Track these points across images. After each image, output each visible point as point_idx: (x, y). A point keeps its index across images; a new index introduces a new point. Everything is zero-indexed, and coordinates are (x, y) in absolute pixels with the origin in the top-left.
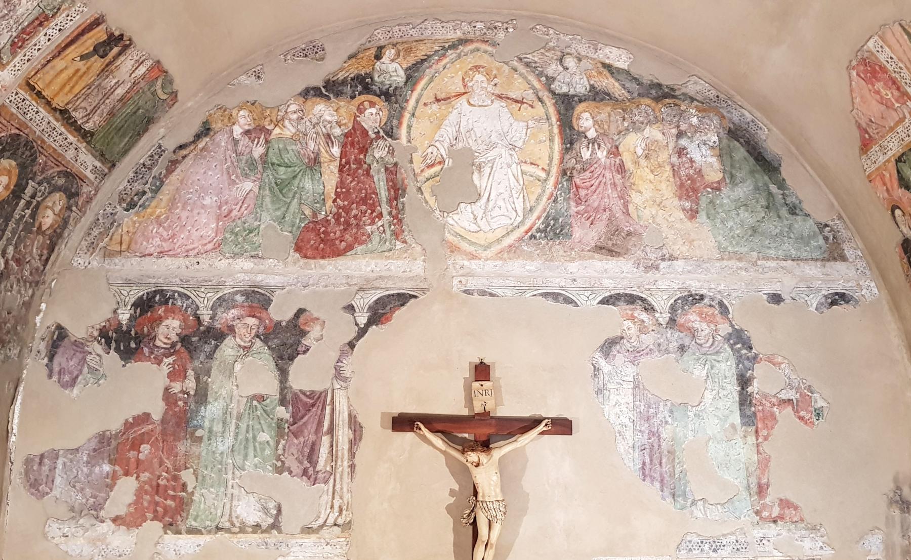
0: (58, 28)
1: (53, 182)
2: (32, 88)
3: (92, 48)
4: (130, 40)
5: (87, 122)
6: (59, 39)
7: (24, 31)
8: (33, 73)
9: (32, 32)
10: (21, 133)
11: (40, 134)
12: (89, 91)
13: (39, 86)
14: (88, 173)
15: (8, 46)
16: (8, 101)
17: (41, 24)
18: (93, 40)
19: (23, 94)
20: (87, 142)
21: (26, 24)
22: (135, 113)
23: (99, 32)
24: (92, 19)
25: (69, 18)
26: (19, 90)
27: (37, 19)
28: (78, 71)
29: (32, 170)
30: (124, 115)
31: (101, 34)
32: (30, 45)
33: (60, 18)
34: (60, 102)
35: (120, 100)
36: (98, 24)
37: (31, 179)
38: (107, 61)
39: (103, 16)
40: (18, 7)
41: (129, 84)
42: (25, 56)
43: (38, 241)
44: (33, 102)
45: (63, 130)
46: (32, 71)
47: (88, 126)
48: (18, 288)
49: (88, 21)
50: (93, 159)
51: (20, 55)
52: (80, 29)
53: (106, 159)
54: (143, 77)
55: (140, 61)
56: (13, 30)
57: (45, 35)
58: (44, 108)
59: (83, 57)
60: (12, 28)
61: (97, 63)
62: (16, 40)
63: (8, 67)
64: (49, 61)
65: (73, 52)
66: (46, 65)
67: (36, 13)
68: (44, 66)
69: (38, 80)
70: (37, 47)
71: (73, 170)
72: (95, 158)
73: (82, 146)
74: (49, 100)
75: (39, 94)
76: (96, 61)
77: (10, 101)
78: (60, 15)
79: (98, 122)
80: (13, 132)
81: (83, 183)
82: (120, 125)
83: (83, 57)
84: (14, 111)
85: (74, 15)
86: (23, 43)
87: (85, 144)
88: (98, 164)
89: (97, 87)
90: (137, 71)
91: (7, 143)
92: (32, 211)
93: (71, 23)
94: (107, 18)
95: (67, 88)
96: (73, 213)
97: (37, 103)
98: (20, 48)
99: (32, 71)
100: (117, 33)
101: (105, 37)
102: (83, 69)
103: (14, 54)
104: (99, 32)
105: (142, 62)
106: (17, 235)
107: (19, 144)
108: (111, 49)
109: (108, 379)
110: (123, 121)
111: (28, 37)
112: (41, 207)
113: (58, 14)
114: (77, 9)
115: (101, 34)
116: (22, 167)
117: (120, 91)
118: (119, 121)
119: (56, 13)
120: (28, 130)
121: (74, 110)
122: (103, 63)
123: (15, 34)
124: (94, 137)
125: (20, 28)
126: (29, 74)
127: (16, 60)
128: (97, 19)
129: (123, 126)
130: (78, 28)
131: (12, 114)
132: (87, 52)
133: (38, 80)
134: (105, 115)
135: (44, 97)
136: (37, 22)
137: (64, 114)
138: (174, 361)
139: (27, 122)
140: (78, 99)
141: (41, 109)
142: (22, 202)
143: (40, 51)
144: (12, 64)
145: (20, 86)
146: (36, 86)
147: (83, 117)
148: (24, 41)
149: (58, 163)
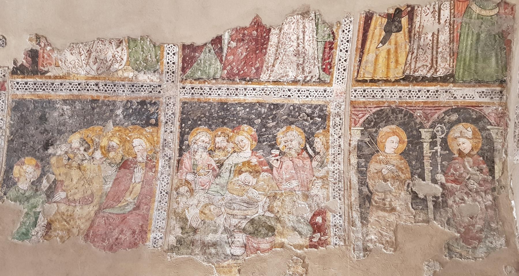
0: (345, 41)
1: (446, 121)
2: (364, 81)
3: (384, 33)
4: (408, 6)
5: (436, 71)
6: (353, 46)
7: (323, 59)
8: (356, 74)
9: (330, 56)
10: (383, 108)
11: (400, 100)
12: (415, 55)
13: (368, 77)
14: (477, 99)
15: (322, 72)
16: (353, 98)
17: (331, 49)
18: (378, 28)
19: (360, 88)
20: (452, 83)
21: (321, 55)
22: (478, 39)
23: (376, 22)
24: (363, 19)
25: (346, 31)
26: (355, 88)
27: (325, 48)
28: (389, 51)
29: (416, 124)
30: (469, 47)
31: (380, 20)
32: (336, 63)
33: (340, 36)
34: (396, 73)
35: (452, 41)
36: (371, 18)
37: (419, 128)
38: (407, 30)
39: (369, 12)
40: (307, 52)
41: (447, 29)
42: (339, 70)
43: (468, 162)
44: (372, 88)
45: (419, 88)
46: (354, 74)
47: (441, 73)
48: (470, 199)
49: (362, 22)
50: (474, 89)
51: (335, 72)
52: (361, 31)
53: (487, 82)
54: (453, 15)
55: (437, 9)
56: (317, 63)
57: (341, 51)
58: (385, 86)
59: (383, 42)
60: (314, 63)
61: (400, 37)
62: (324, 67)
63: (334, 82)
64: (360, 61)
65: (371, 45)
66: (360, 64)
67: (321, 46)
68: (359, 66)
69: (364, 74)
70: (342, 60)
71: (459, 105)
72: (474, 87)
73: (450, 87)
74: (385, 79)
75: (373, 81)
76: (396, 37)
77: (355, 97)
78: (338, 35)
79: (447, 66)
80: (374, 110)
81: (480, 108)
82: (474, 54)
83: (383, 42)
84: (364, 100)
85: (347, 28)
86: (331, 65)
87: (451, 85)
88: (480, 89)
89: (418, 48)
90: (442, 17)
91: (375, 119)
92: (440, 145)
93: (351, 33)
94: (372, 10)
95: (392, 65)
96: (491, 130)
97: (376, 86)
98: (330, 68)
99: (354, 74)
100: (392, 11)
101: (385, 21)
102: (392, 47)
103: (330, 74)
104: (376, 22)
105: (440, 9)
106: (439, 166)
107: (387, 114)
108: (400, 22)
109: (398, 252)
110: (473, 51)
111: (330, 60)
112: (449, 141)
113: (336, 35)
114: (345, 23)
115: (380, 20)
116: (404, 125)
117: (444, 37)
118: (468, 54)
119: (334, 36)
120: (386, 103)
121: (414, 72)
122: (405, 33)
123: (320, 65)
124: (456, 76)
125: (319, 59)
126: (353, 76)
127: (334, 76)
128: (366, 16)
129: (477, 54)
130: (359, 31)
131: (364, 102)
132: (382, 37)
133: (364, 74)
134: (448, 58)
135: (379, 80)
136: (327, 50)
137: (407, 79)
138: (330, 212)
139: (381, 100)
140: (410, 64)
141: (383, 88)
142: (426, 146)
143: (348, 61)
144: (334, 79)
145: (353, 85)
146: (366, 79)
147: (428, 72)
148: (330, 64)
149: (438, 108)
